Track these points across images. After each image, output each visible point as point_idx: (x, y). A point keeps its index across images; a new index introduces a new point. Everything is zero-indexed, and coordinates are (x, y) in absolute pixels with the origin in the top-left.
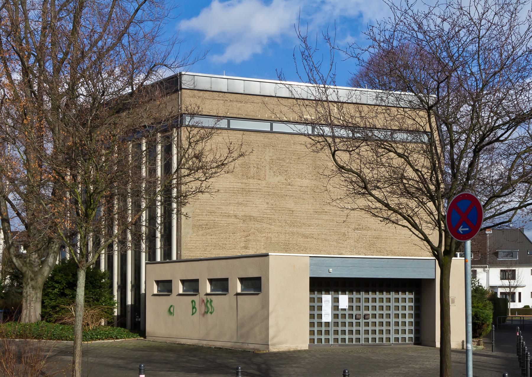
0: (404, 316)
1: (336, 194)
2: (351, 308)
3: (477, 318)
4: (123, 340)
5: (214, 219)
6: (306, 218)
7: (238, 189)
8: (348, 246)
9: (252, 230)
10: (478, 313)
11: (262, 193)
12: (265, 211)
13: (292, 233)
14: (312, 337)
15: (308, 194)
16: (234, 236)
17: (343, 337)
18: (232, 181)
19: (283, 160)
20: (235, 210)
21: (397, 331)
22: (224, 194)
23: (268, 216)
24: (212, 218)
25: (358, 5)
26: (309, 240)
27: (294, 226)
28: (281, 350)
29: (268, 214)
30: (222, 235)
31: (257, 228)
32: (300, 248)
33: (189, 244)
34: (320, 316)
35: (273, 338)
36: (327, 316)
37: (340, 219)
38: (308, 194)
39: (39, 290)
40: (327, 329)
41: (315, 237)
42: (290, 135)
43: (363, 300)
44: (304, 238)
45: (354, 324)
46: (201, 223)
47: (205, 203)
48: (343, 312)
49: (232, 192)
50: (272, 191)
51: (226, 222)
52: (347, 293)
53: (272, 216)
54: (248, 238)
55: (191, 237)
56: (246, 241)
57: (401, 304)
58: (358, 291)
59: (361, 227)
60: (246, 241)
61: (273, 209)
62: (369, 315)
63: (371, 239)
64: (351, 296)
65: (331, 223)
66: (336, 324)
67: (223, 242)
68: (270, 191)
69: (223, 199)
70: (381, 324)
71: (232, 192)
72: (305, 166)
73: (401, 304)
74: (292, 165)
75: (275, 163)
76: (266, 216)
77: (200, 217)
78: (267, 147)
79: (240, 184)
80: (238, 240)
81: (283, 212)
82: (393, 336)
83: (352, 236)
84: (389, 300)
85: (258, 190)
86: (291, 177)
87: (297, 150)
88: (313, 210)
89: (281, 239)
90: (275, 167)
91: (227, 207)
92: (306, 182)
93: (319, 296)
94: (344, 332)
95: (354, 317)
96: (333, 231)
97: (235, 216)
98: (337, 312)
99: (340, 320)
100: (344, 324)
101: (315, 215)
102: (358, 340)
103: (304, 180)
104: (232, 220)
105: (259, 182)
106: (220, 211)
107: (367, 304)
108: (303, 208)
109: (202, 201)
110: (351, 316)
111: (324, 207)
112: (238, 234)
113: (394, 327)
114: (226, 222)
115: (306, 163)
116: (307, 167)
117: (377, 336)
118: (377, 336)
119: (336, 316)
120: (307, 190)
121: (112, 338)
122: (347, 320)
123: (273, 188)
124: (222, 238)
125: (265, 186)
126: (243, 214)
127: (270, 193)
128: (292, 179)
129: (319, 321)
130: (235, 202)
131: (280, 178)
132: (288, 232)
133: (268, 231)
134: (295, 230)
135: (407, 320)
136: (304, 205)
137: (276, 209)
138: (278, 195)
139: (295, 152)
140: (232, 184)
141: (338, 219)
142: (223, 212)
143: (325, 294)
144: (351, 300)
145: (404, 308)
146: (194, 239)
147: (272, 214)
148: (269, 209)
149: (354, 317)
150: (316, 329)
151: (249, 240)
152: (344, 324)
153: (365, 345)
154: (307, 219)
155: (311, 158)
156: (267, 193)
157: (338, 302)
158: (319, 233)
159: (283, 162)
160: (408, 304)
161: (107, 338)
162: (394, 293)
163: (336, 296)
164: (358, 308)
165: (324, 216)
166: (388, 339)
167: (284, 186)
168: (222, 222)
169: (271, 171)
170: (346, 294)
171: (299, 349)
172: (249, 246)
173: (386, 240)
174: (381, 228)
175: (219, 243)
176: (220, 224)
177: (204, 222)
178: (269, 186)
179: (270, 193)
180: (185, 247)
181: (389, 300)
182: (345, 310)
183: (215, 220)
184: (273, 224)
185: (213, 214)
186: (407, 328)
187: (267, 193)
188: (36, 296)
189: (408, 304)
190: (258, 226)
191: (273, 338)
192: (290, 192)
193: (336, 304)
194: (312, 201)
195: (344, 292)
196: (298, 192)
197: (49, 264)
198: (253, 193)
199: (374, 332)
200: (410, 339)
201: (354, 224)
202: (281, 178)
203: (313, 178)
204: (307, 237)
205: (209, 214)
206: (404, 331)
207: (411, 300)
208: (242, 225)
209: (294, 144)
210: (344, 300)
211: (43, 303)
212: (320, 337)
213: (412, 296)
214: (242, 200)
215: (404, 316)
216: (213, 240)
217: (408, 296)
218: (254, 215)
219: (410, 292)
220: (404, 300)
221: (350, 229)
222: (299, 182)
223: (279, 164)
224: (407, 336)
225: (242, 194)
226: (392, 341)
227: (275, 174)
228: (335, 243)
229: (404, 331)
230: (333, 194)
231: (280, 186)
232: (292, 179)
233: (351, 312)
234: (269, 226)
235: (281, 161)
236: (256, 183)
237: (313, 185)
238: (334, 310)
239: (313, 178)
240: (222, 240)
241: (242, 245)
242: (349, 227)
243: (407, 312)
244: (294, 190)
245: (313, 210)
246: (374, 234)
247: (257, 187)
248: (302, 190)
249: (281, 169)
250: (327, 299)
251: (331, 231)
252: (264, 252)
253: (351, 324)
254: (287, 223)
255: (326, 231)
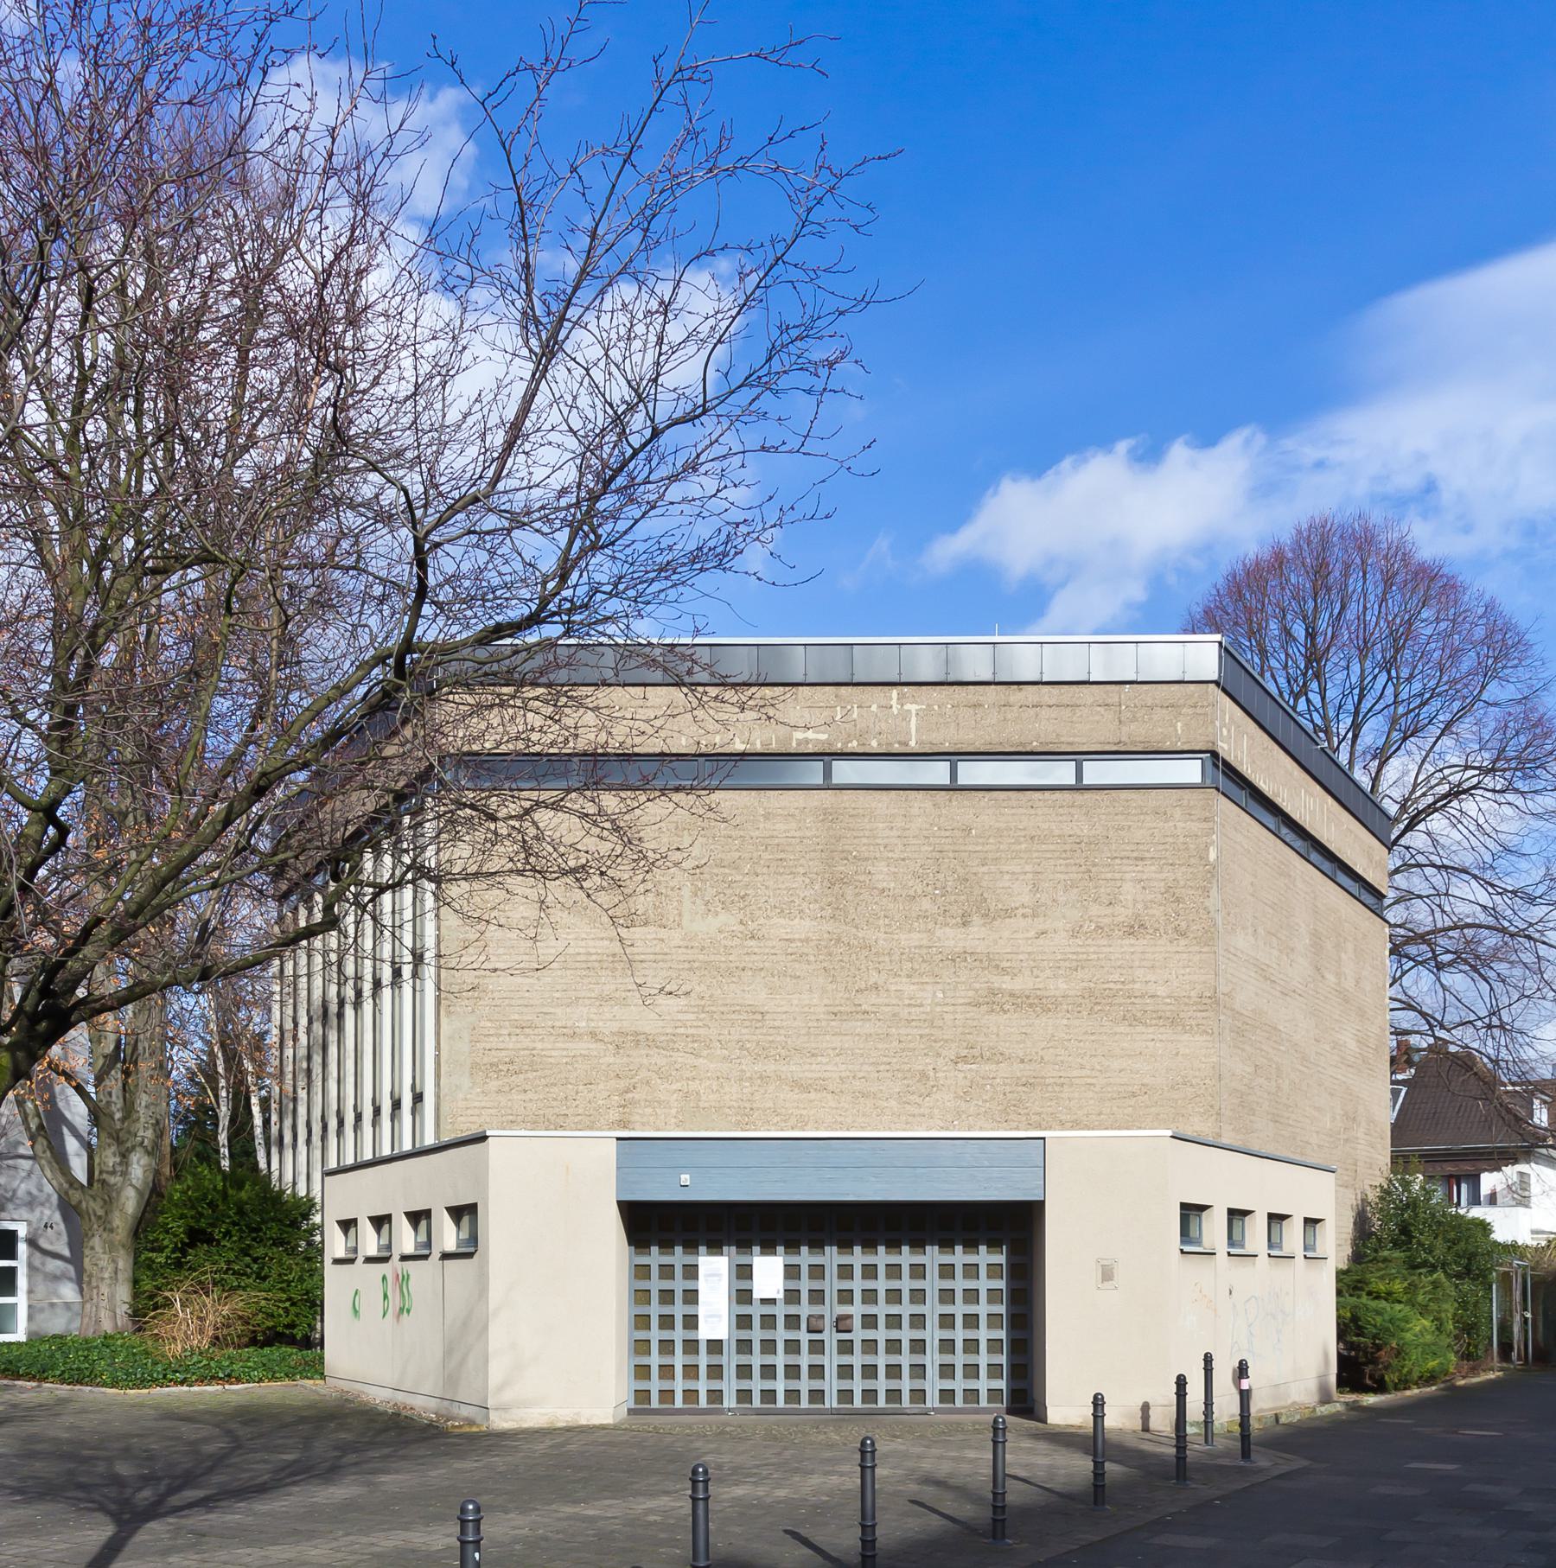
0: (971, 1321)
1: (896, 957)
2: (792, 1296)
3: (1359, 1328)
4: (251, 1385)
5: (531, 1045)
6: (803, 1032)
7: (599, 958)
8: (936, 1111)
9: (643, 1074)
10: (1361, 1313)
11: (669, 964)
12: (680, 1016)
13: (761, 1078)
14: (642, 1385)
15: (809, 962)
16: (590, 1092)
17: (768, 1385)
18: (584, 936)
19: (734, 865)
20: (592, 1016)
21: (845, 1371)
22: (559, 973)
23: (691, 1031)
24: (526, 1043)
25: (1421, 457)
26: (813, 1096)
27: (767, 1057)
28: (525, 1425)
29: (689, 1024)
30: (555, 1089)
31: (656, 1068)
32: (785, 1121)
33: (462, 1119)
34: (691, 1322)
35: (501, 1388)
36: (715, 1319)
37: (909, 1031)
38: (809, 962)
39: (122, 1252)
40: (715, 1360)
41: (831, 1088)
42: (753, 793)
43: (831, 1272)
44: (796, 1091)
45: (805, 1347)
46: (494, 1057)
47: (507, 1001)
48: (768, 1310)
49: (584, 965)
50: (701, 957)
51: (565, 1053)
52: (780, 1249)
53: (702, 1031)
54: (630, 1095)
55: (466, 1099)
56: (624, 1106)
57: (960, 1284)
58: (817, 1245)
59: (976, 1052)
60: (624, 1106)
61: (702, 1009)
62: (850, 1317)
63: (1008, 1089)
64: (794, 1260)
65: (880, 1046)
66: (744, 1346)
67: (557, 1110)
68: (695, 957)
69: (558, 987)
70: (894, 1346)
71: (584, 965)
72: (800, 879)
73: (960, 1284)
74: (760, 878)
75: (708, 877)
76: (682, 1030)
77: (493, 1042)
78: (686, 832)
79: (606, 943)
80: (601, 1102)
81: (733, 1016)
82: (933, 1384)
83: (949, 1082)
84: (918, 1271)
85: (660, 957)
86: (758, 913)
87: (775, 833)
88: (824, 1009)
89: (727, 1097)
90: (709, 889)
91: (568, 1010)
92: (802, 927)
93: (689, 1260)
94: (769, 1371)
95: (804, 1326)
96: (888, 1067)
97: (593, 1035)
98: (745, 1310)
99: (757, 1334)
100: (769, 1346)
101: (833, 1023)
102: (817, 1395)
103: (797, 921)
104: (583, 1046)
105: (663, 933)
106: (550, 1023)
107: (846, 1285)
108: (795, 1002)
109: (496, 995)
110: (792, 1321)
111: (860, 999)
112: (601, 1086)
113: (937, 1356)
114: (565, 1053)
115: (802, 871)
116: (807, 881)
117: (882, 1384)
118: (882, 1384)
119: (743, 1322)
120: (806, 951)
121: (214, 1378)
122: (781, 1334)
123: (703, 948)
124: (555, 1099)
125: (681, 943)
126: (615, 1027)
127: (696, 965)
128: (762, 921)
129: (690, 1335)
130: (593, 995)
131: (723, 917)
132: (748, 1075)
133: (688, 1075)
134: (770, 1068)
135: (983, 1334)
136: (797, 996)
137: (713, 1009)
138: (718, 970)
139: (768, 841)
140: (583, 944)
141: (903, 1031)
142: (557, 1024)
143: (710, 1254)
144: (791, 1272)
145: (972, 1296)
146: (476, 1104)
147: (700, 1024)
148: (691, 1010)
149: (804, 1326)
150: (655, 1360)
151: (633, 1102)
152: (769, 1346)
153: (838, 1412)
154: (808, 1034)
155: (818, 854)
156: (687, 965)
157: (751, 1278)
158: (843, 1074)
159: (733, 872)
160: (984, 1284)
161: (202, 1380)
162: (835, 1248)
163: (743, 1260)
164: (817, 1296)
165: (859, 1024)
166: (919, 1395)
167: (737, 941)
168: (554, 1053)
169: (698, 901)
170: (775, 1254)
171: (583, 1422)
172: (632, 1119)
173: (1057, 1089)
174: (1040, 1053)
175: (547, 1111)
176: (550, 1060)
177: (504, 1053)
178: (690, 944)
179: (696, 965)
180: (449, 1127)
181: (918, 1271)
182: (772, 1301)
183: (534, 1049)
184: (705, 1053)
185: (527, 1031)
186: (983, 1359)
187: (687, 965)
188: (112, 1265)
189: (984, 1284)
190: (658, 1059)
191: (501, 1388)
192: (756, 958)
193: (744, 1285)
194: (821, 980)
195: (768, 1248)
196: (779, 958)
197: (134, 1182)
198: (644, 965)
199: (870, 1371)
200: (994, 1394)
201: (954, 1046)
202: (727, 919)
203: (824, 913)
204: (806, 1089)
205: (518, 1031)
206: (972, 1371)
207: (994, 1271)
208: (612, 1060)
209: (767, 816)
210: (769, 1273)
211: (136, 1282)
212: (691, 1385)
213: (1001, 1259)
214: (613, 987)
215: (971, 1321)
216: (529, 1105)
217: (985, 1257)
218: (647, 1030)
219: (993, 1244)
220: (971, 1271)
221: (940, 1061)
222: (779, 927)
223: (720, 878)
224: (983, 1384)
225: (614, 970)
226: (933, 1400)
227: (710, 907)
228: (893, 1103)
229: (972, 1371)
230: (887, 959)
231: (723, 942)
232: (762, 921)
233: (793, 1310)
234: (691, 1060)
235: (727, 871)
236: (654, 936)
237: (826, 936)
238: (738, 1303)
239: (824, 913)
240: (555, 1103)
241: (614, 1115)
242: (939, 1055)
243: (983, 1309)
244: (767, 951)
245: (824, 1009)
246: (1019, 1074)
247: (657, 950)
248: (790, 951)
249: (728, 892)
250: (714, 1270)
251: (882, 1068)
252: (473, 1130)
253: (793, 1347)
254: (747, 1049)
255: (866, 1068)
